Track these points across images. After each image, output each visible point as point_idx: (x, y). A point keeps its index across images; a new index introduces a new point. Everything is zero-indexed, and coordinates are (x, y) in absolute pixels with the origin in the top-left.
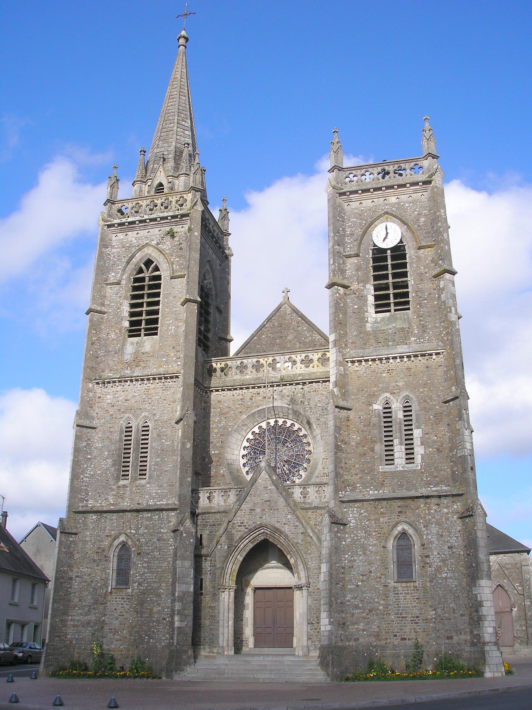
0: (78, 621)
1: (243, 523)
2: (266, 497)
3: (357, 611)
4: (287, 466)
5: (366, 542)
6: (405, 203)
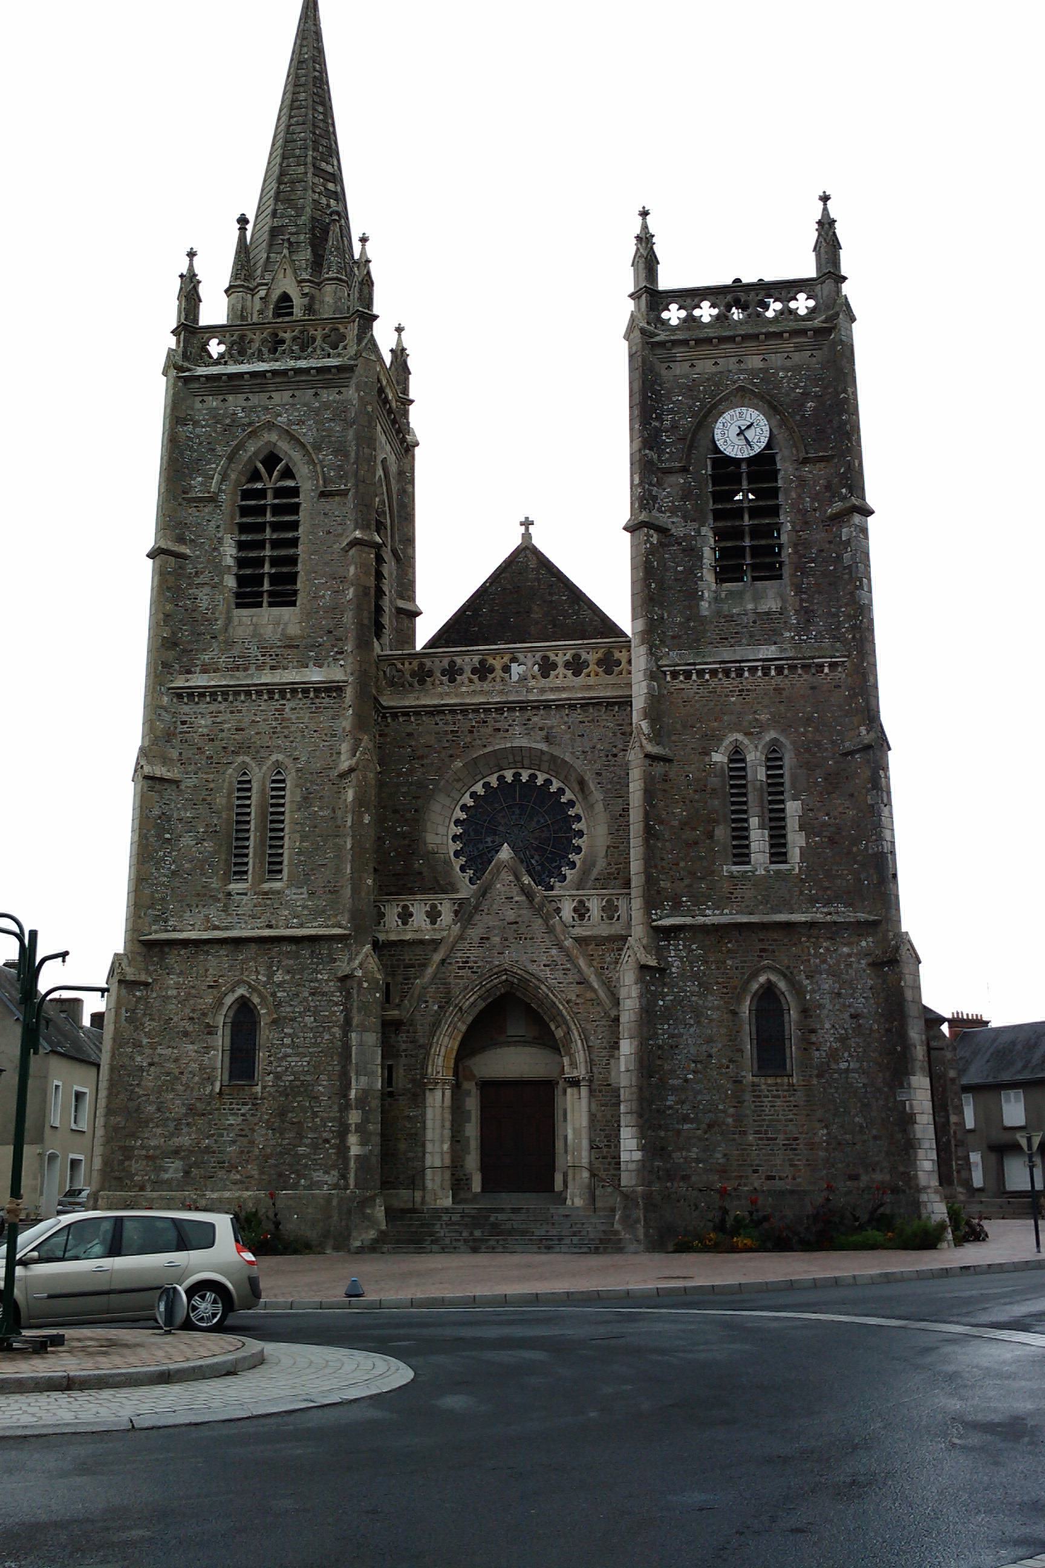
0: (155, 1148)
1: (467, 962)
2: (510, 915)
3: (686, 1127)
4: (537, 857)
5: (701, 1002)
6: (777, 370)
